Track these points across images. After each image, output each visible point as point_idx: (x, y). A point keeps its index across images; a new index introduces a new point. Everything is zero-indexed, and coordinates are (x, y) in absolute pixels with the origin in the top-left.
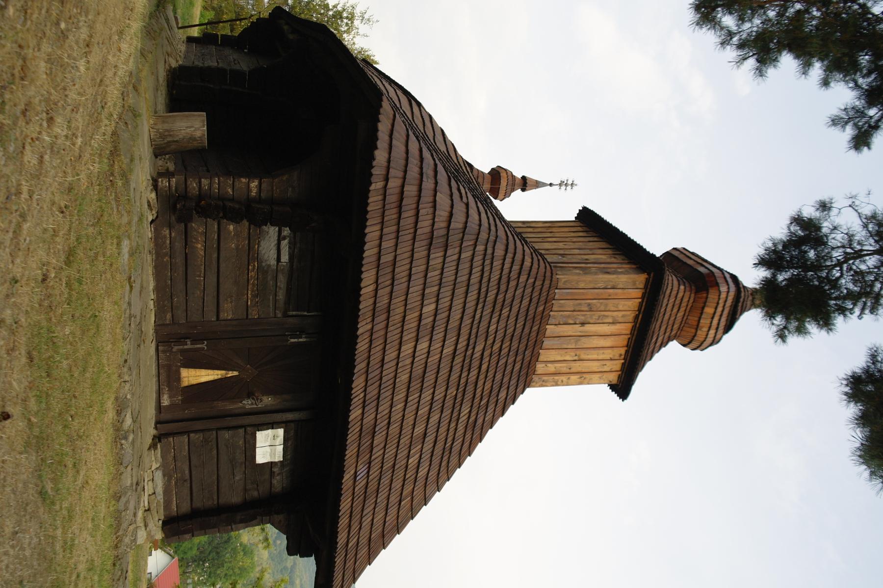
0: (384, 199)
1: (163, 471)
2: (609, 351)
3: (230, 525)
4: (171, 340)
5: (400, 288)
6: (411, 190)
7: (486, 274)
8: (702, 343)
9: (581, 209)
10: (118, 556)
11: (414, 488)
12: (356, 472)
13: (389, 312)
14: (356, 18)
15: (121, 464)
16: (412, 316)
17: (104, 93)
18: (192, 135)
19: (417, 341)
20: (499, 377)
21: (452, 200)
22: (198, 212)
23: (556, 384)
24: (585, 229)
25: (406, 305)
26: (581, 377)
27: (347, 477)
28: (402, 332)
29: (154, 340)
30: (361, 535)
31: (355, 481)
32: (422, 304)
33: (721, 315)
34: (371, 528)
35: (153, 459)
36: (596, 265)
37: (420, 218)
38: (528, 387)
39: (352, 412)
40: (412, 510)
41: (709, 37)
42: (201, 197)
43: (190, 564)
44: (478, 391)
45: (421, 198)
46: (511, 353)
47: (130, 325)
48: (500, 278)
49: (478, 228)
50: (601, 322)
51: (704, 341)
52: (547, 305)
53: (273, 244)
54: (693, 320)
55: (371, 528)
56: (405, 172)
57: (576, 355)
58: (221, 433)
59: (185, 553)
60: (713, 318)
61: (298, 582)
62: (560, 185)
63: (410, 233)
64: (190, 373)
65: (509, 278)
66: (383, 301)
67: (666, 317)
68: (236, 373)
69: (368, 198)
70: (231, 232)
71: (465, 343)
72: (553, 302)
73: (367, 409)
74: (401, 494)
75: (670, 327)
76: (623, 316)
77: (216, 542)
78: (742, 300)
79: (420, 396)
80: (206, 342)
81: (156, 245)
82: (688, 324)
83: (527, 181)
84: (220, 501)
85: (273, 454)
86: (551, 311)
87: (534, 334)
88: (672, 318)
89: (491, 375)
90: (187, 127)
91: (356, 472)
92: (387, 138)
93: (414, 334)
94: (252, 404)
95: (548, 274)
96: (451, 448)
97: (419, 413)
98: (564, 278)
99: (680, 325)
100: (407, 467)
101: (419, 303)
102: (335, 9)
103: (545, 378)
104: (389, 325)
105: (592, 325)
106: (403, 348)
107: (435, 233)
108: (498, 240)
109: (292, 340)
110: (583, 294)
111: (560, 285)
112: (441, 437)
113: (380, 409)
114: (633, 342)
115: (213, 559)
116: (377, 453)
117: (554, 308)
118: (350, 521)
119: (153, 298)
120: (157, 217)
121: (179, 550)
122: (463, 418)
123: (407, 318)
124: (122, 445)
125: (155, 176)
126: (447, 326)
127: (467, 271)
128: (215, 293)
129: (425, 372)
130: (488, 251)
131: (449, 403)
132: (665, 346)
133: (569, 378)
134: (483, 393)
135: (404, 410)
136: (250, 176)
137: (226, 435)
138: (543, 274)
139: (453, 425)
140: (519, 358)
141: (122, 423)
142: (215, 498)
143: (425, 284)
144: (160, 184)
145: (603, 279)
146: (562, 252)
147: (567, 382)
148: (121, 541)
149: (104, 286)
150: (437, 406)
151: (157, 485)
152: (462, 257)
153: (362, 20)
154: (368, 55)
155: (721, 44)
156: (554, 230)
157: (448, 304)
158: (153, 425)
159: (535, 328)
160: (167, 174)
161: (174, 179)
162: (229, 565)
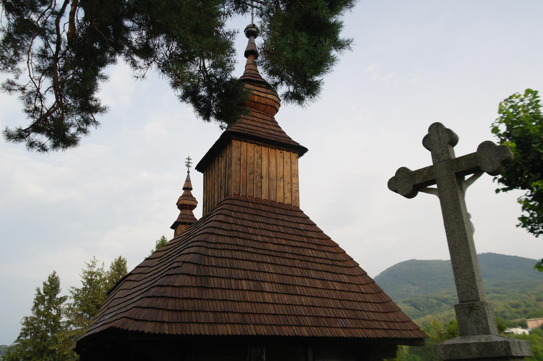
2: (278, 159)
6: (171, 304)
7: (226, 247)
13: (244, 313)
19: (264, 291)
20: (290, 231)
23: (298, 191)
28: (257, 302)
32: (241, 290)
33: (259, 91)
34: (377, 312)
37: (189, 296)
38: (299, 208)
44: (298, 245)
49: (198, 255)
50: (260, 166)
56: (160, 309)
57: (280, 180)
60: (261, 96)
61: (445, 296)
63: (197, 303)
67: (259, 125)
75: (265, 122)
76: (257, 153)
78: (251, 78)
82: (264, 110)
83: (186, 187)
86: (253, 197)
87: (267, 208)
88: (260, 120)
89: (288, 237)
91: (341, 328)
92: (138, 323)
93: (260, 293)
98: (233, 191)
99: (265, 114)
102: (86, 284)
103: (294, 198)
105: (262, 171)
107: (199, 285)
108: (206, 240)
110: (243, 178)
111: (237, 192)
112: (324, 267)
114: (273, 146)
116: (331, 313)
117: (252, 195)
122: (314, 253)
126: (256, 271)
130: (212, 247)
133: (294, 183)
139: (318, 260)
140: (280, 217)
143: (229, 289)
145: (234, 167)
146: (219, 188)
153: (93, 267)
154: (115, 263)
157: (242, 271)
159: (263, 207)
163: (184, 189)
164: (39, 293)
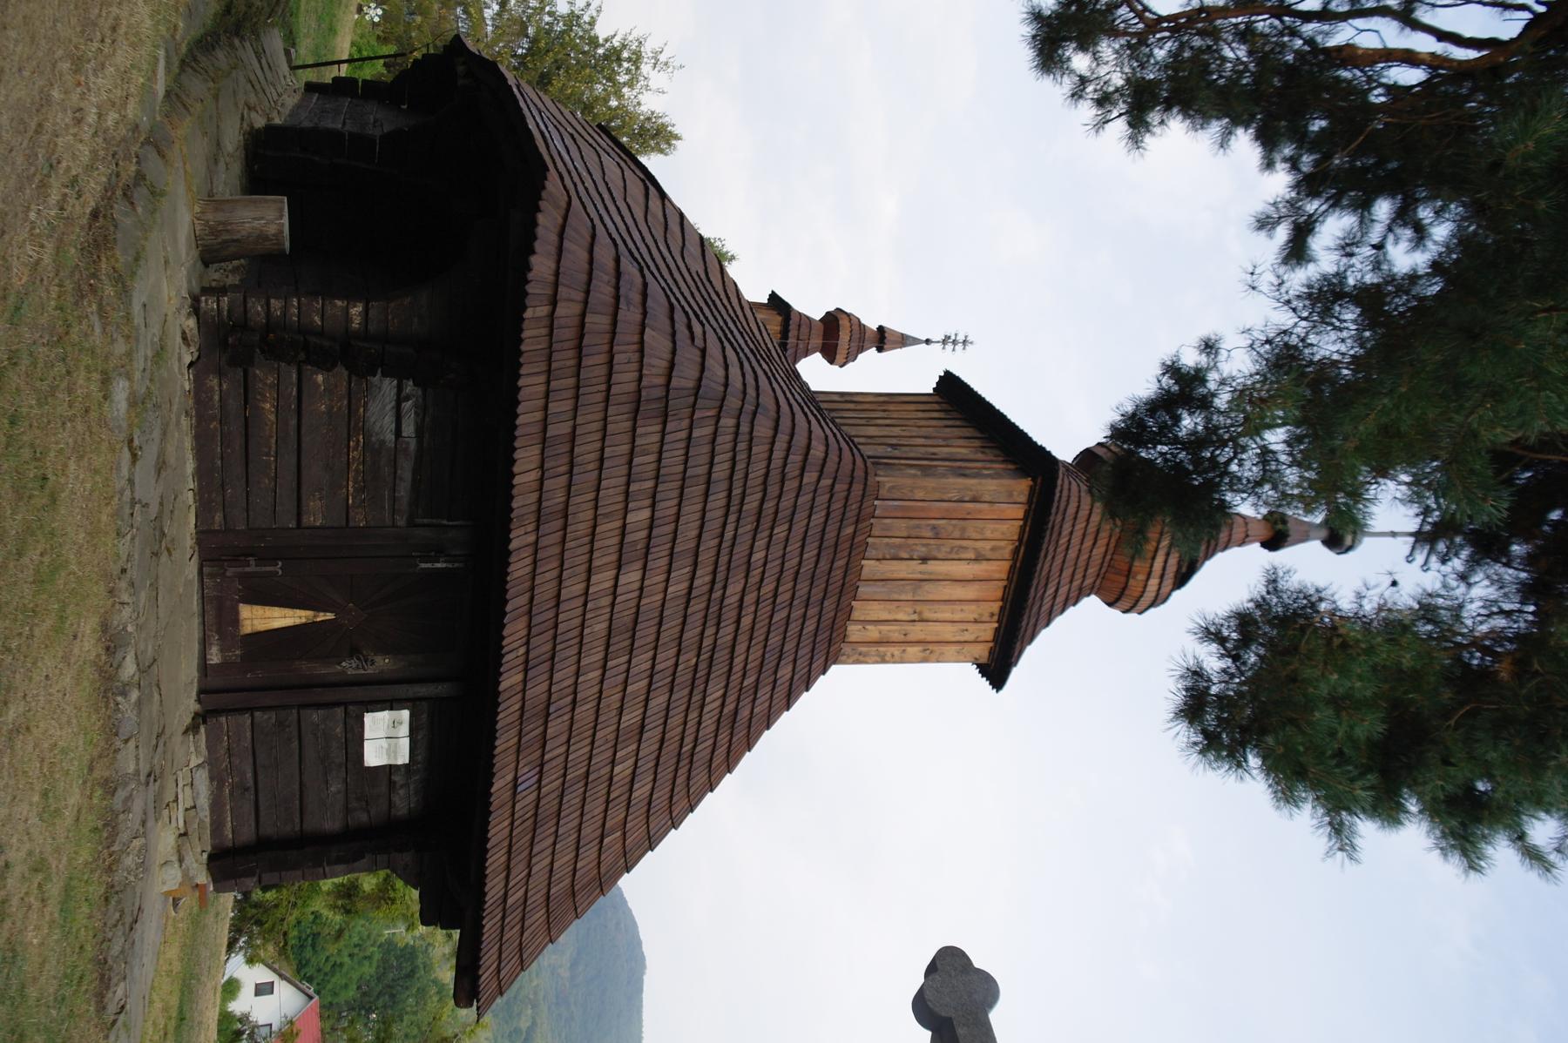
0: (551, 334)
1: (210, 771)
2: (973, 607)
3: (320, 866)
4: (224, 558)
5: (586, 479)
6: (598, 321)
7: (740, 466)
8: (1137, 601)
9: (942, 374)
10: (113, 886)
11: (626, 817)
12: (516, 779)
13: (566, 517)
14: (645, 60)
15: (116, 734)
16: (609, 527)
17: (51, 146)
18: (262, 231)
19: (619, 568)
20: (775, 640)
21: (674, 342)
22: (263, 352)
24: (945, 406)
25: (596, 508)
26: (925, 650)
27: (500, 784)
28: (591, 552)
29: (196, 553)
30: (530, 887)
31: (515, 794)
34: (550, 877)
35: (192, 749)
36: (947, 463)
37: (616, 368)
38: (835, 663)
39: (505, 676)
40: (625, 856)
41: (1055, 89)
42: (270, 326)
43: (345, 1014)
45: (617, 337)
46: (795, 603)
47: (132, 514)
48: (767, 475)
49: (722, 389)
51: (1141, 596)
52: (860, 526)
53: (389, 407)
55: (550, 877)
56: (588, 292)
57: (915, 612)
58: (305, 713)
59: (335, 994)
62: (944, 342)
63: (599, 391)
64: (255, 612)
65: (783, 474)
66: (555, 499)
67: (1072, 554)
68: (330, 616)
69: (521, 330)
70: (320, 386)
71: (708, 579)
72: (872, 521)
73: (531, 674)
74: (604, 825)
76: (993, 549)
77: (391, 975)
79: (629, 662)
80: (280, 563)
81: (198, 401)
83: (886, 335)
84: (304, 826)
85: (392, 751)
86: (869, 536)
87: (837, 574)
88: (1084, 557)
90: (254, 219)
91: (516, 779)
93: (614, 557)
94: (358, 668)
95: (859, 473)
96: (692, 755)
97: (630, 689)
98: (888, 482)
100: (611, 779)
101: (621, 506)
103: (863, 649)
104: (568, 540)
105: (941, 562)
106: (594, 579)
108: (759, 410)
109: (423, 565)
110: (923, 509)
111: (883, 493)
112: (674, 734)
113: (557, 677)
115: (385, 1007)
116: (555, 750)
118: (509, 860)
119: (192, 487)
120: (199, 357)
121: (324, 988)
122: (712, 706)
123: (598, 530)
124: (117, 704)
125: (197, 291)
127: (705, 459)
128: (294, 484)
129: (636, 622)
131: (684, 676)
132: (1075, 604)
133: (904, 651)
134: (746, 664)
135: (602, 682)
136: (351, 298)
137: (315, 716)
138: (848, 472)
139: (693, 715)
140: (813, 611)
141: (117, 669)
142: (297, 820)
143: (629, 475)
144: (203, 305)
146: (894, 441)
147: (901, 658)
148: (117, 861)
149: (71, 440)
150: (662, 681)
151: (198, 794)
152: (694, 435)
153: (655, 64)
154: (663, 124)
155: (1073, 95)
156: (891, 407)
158: (194, 694)
159: (840, 563)
160: (218, 291)
161: (226, 299)
162: (414, 1018)
163: (881, 329)
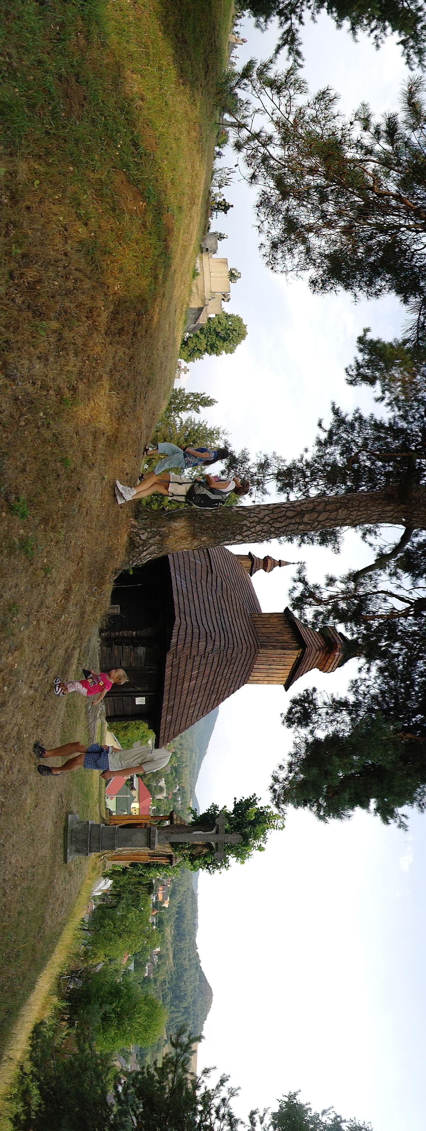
54: (324, 663)
136: (133, 631)
163: (280, 561)
164: (202, 395)
